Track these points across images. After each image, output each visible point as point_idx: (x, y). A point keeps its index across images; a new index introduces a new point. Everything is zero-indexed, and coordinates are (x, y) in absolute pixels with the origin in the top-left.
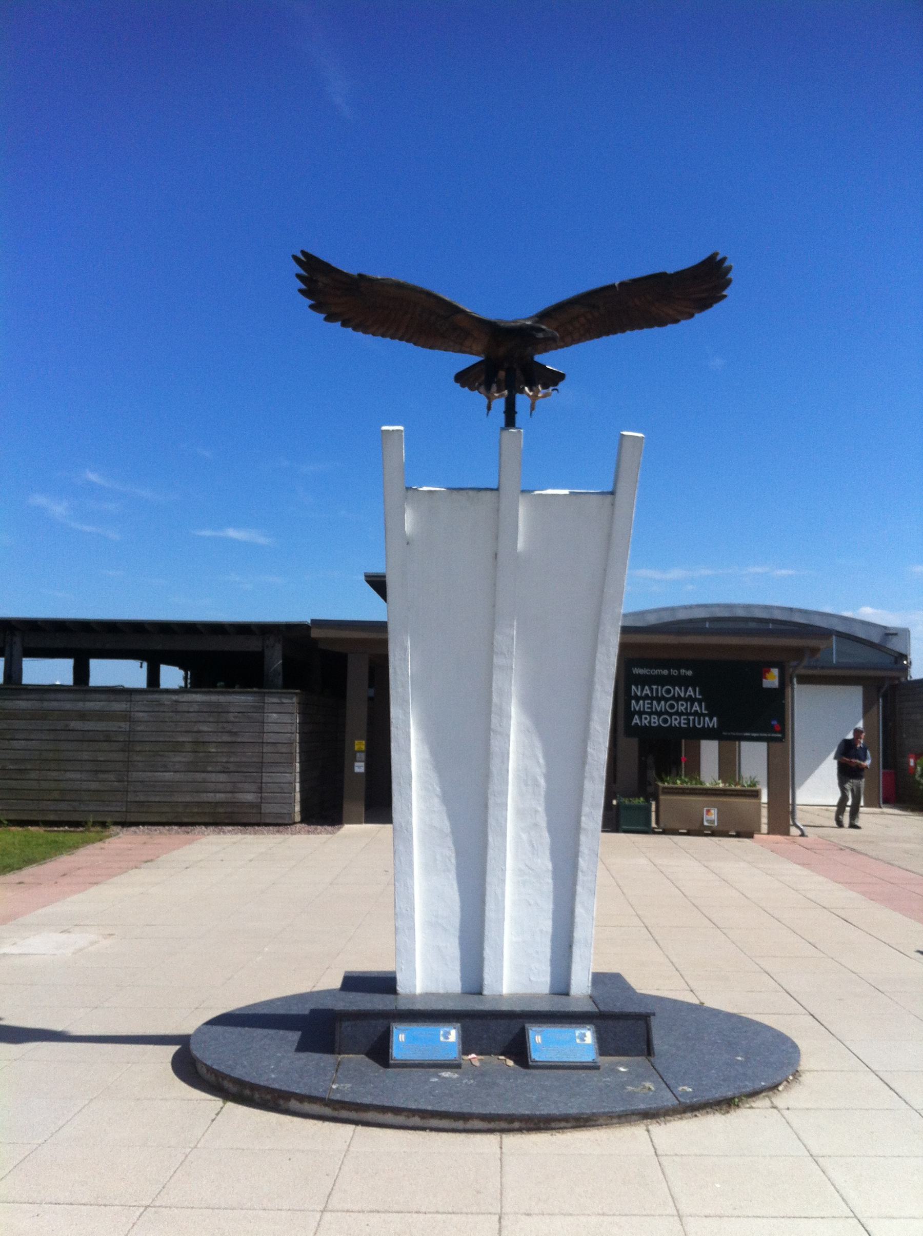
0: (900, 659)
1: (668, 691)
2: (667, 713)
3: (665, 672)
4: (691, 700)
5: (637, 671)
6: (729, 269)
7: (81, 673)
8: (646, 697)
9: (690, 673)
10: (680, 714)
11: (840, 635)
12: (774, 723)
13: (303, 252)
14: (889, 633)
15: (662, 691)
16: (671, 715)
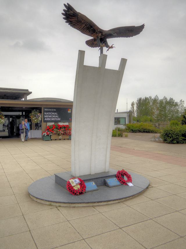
1: (51, 114)
2: (51, 118)
3: (51, 110)
4: (56, 115)
5: (45, 110)
8: (47, 115)
10: (53, 118)
13: (68, 4)
15: (50, 113)
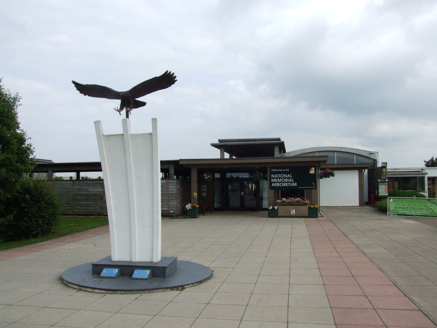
0: (375, 161)
1: (282, 176)
3: (281, 170)
4: (289, 178)
5: (273, 170)
6: (175, 77)
7: (78, 175)
9: (288, 170)
11: (356, 154)
12: (313, 184)
14: (371, 153)
15: (280, 176)
16: (283, 183)
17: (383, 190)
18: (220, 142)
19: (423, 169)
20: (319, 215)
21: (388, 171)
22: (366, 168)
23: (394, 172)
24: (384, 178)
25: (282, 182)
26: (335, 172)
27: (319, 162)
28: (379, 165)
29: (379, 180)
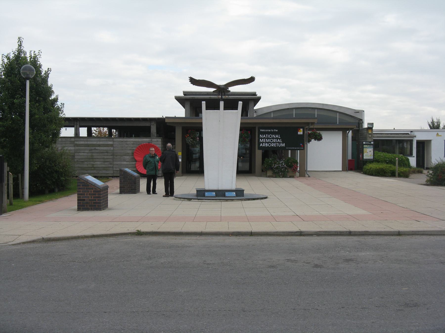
0: (360, 122)
3: (270, 131)
4: (277, 138)
5: (261, 130)
9: (277, 131)
11: (340, 113)
14: (357, 112)
15: (269, 136)
16: (271, 143)
17: (368, 153)
18: (185, 95)
19: (412, 132)
20: (306, 175)
21: (374, 133)
22: (351, 129)
23: (381, 133)
24: (370, 140)
25: (270, 142)
26: (324, 134)
27: (308, 124)
28: (365, 126)
29: (364, 143)
